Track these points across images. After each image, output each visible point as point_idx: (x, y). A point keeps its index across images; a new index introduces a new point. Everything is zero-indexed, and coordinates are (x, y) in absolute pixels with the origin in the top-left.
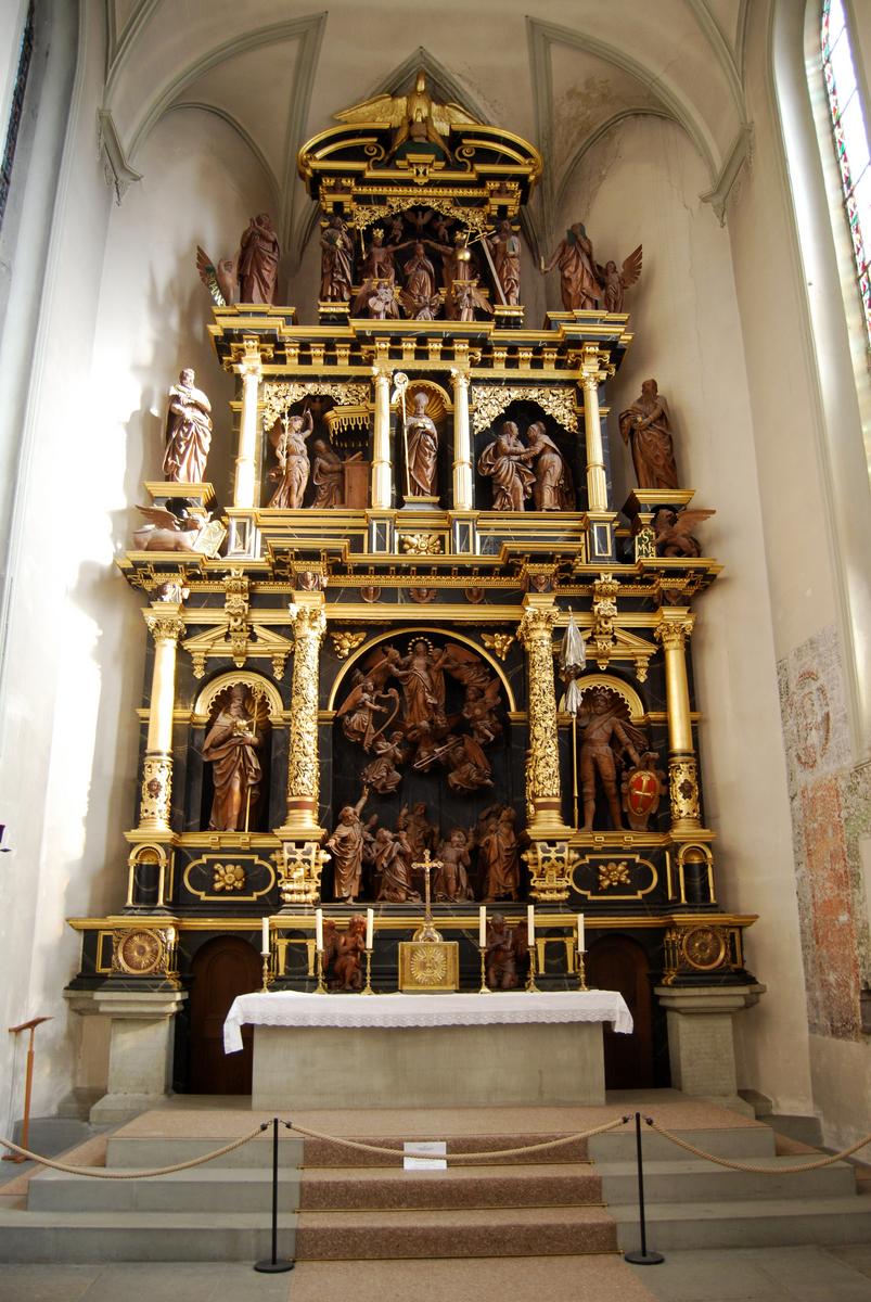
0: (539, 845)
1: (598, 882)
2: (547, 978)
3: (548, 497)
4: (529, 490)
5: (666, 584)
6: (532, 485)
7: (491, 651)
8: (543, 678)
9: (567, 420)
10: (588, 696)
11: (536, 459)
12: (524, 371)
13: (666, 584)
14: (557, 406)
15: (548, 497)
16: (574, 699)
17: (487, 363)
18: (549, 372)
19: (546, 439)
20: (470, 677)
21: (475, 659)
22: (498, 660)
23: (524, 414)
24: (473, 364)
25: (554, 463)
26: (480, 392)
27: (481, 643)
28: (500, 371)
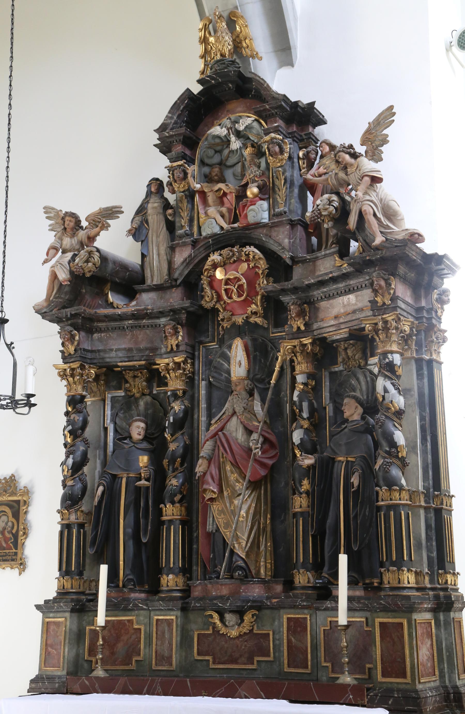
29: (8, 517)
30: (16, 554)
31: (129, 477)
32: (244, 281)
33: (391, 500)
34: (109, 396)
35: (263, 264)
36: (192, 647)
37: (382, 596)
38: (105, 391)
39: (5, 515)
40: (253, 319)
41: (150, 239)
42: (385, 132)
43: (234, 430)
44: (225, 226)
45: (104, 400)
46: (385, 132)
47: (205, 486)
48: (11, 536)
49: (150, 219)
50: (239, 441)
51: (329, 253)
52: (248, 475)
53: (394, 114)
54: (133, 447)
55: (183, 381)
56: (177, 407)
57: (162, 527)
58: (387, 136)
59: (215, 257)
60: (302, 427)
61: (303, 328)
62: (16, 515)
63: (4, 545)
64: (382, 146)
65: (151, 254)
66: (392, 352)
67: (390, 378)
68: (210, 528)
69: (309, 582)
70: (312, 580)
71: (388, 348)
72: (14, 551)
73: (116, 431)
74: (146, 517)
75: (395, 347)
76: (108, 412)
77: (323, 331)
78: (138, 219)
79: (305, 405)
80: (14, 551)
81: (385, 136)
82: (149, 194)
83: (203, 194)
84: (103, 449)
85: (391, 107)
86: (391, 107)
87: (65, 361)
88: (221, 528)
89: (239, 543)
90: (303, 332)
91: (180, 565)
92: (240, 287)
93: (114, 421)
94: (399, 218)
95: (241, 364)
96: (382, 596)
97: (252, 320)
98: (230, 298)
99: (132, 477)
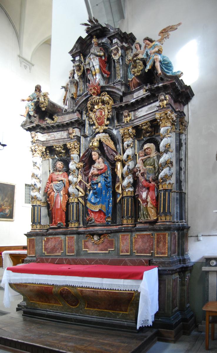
2: (102, 61)
79: (109, 249)
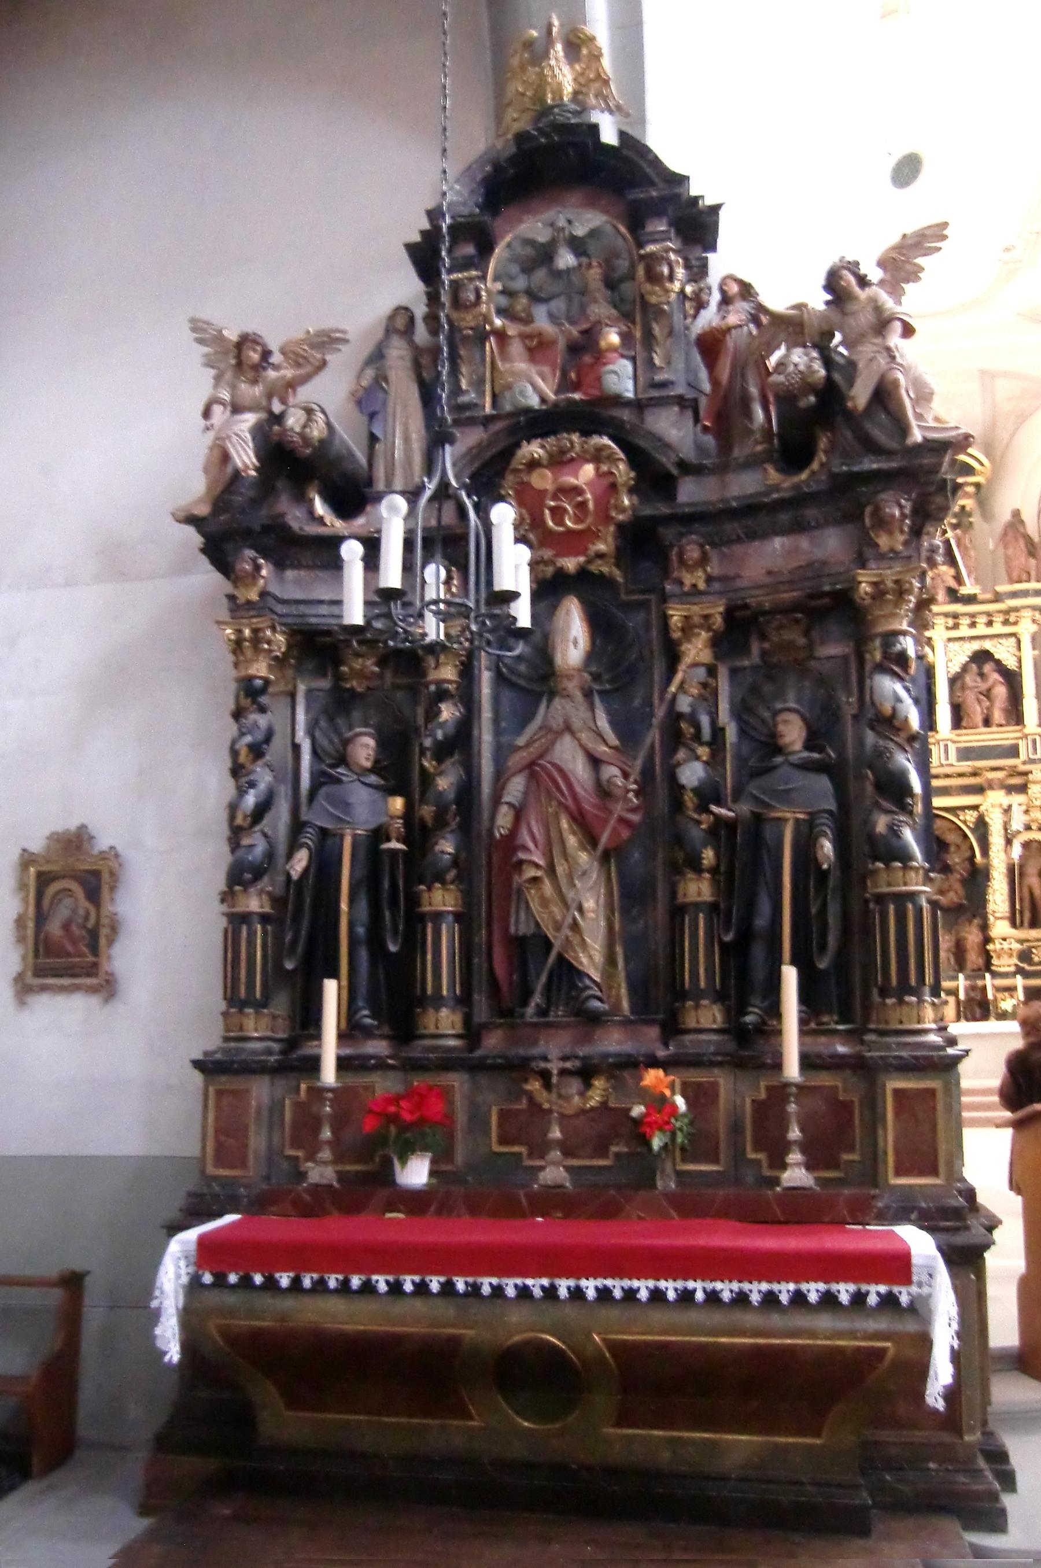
0: (996, 941)
1: (1031, 959)
3: (998, 716)
4: (985, 711)
5: (991, 775)
6: (988, 708)
7: (965, 822)
8: (996, 840)
9: (1011, 663)
10: (1026, 845)
11: (989, 690)
12: (981, 630)
13: (991, 775)
14: (1003, 652)
15: (998, 716)
16: (1017, 851)
17: (956, 626)
18: (998, 628)
19: (996, 676)
20: (951, 838)
21: (954, 826)
22: (968, 826)
23: (982, 657)
24: (948, 628)
25: (1001, 691)
26: (954, 646)
27: (957, 816)
28: (964, 631)
29: (76, 900)
30: (95, 965)
31: (356, 834)
32: (589, 496)
33: (905, 884)
34: (302, 688)
35: (622, 471)
36: (487, 1132)
37: (894, 1046)
38: (295, 679)
39: (71, 896)
40: (596, 567)
41: (390, 410)
42: (920, 261)
43: (570, 757)
44: (552, 396)
45: (293, 696)
46: (920, 261)
47: (522, 855)
48: (84, 933)
49: (392, 376)
50: (580, 778)
51: (411, 449)
52: (604, 839)
53: (944, 237)
54: (357, 783)
55: (456, 666)
56: (448, 712)
57: (419, 926)
58: (921, 269)
59: (534, 449)
60: (697, 758)
61: (702, 586)
62: (94, 895)
63: (70, 948)
64: (907, 281)
65: (389, 436)
66: (904, 633)
67: (901, 679)
68: (522, 927)
69: (714, 1021)
70: (719, 1017)
71: (896, 626)
72: (91, 959)
73: (315, 752)
74: (394, 903)
75: (905, 626)
76: (301, 717)
77: (742, 594)
78: (370, 373)
80: (91, 959)
81: (916, 269)
82: (390, 330)
83: (501, 336)
84: (290, 786)
85: (945, 225)
86: (945, 225)
87: (334, 610)
88: (548, 930)
89: (590, 957)
90: (701, 593)
91: (458, 992)
92: (583, 505)
93: (311, 732)
94: (604, 360)
95: (577, 642)
96: (894, 1046)
97: (593, 568)
98: (560, 522)
99: (360, 835)
